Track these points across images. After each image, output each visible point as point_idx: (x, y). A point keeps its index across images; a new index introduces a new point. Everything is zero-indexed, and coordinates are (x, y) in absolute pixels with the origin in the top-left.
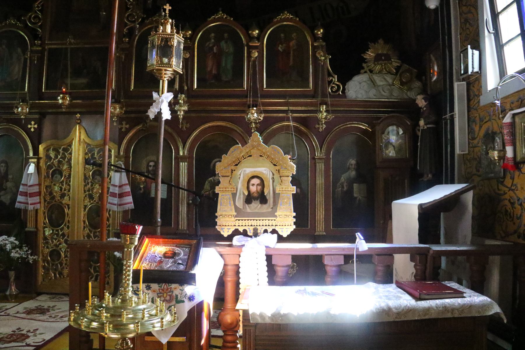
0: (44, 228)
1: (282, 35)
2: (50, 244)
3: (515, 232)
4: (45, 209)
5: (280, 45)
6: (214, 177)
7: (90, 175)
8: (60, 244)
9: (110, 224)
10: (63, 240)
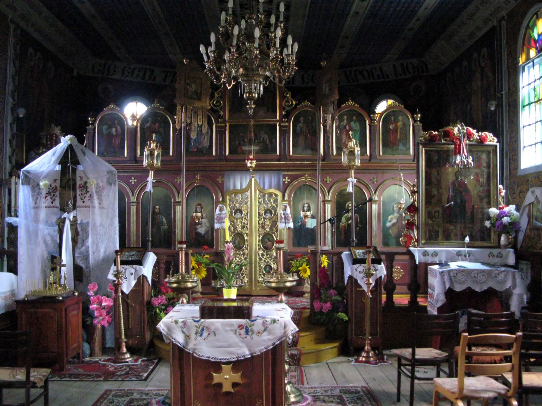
3: (532, 246)
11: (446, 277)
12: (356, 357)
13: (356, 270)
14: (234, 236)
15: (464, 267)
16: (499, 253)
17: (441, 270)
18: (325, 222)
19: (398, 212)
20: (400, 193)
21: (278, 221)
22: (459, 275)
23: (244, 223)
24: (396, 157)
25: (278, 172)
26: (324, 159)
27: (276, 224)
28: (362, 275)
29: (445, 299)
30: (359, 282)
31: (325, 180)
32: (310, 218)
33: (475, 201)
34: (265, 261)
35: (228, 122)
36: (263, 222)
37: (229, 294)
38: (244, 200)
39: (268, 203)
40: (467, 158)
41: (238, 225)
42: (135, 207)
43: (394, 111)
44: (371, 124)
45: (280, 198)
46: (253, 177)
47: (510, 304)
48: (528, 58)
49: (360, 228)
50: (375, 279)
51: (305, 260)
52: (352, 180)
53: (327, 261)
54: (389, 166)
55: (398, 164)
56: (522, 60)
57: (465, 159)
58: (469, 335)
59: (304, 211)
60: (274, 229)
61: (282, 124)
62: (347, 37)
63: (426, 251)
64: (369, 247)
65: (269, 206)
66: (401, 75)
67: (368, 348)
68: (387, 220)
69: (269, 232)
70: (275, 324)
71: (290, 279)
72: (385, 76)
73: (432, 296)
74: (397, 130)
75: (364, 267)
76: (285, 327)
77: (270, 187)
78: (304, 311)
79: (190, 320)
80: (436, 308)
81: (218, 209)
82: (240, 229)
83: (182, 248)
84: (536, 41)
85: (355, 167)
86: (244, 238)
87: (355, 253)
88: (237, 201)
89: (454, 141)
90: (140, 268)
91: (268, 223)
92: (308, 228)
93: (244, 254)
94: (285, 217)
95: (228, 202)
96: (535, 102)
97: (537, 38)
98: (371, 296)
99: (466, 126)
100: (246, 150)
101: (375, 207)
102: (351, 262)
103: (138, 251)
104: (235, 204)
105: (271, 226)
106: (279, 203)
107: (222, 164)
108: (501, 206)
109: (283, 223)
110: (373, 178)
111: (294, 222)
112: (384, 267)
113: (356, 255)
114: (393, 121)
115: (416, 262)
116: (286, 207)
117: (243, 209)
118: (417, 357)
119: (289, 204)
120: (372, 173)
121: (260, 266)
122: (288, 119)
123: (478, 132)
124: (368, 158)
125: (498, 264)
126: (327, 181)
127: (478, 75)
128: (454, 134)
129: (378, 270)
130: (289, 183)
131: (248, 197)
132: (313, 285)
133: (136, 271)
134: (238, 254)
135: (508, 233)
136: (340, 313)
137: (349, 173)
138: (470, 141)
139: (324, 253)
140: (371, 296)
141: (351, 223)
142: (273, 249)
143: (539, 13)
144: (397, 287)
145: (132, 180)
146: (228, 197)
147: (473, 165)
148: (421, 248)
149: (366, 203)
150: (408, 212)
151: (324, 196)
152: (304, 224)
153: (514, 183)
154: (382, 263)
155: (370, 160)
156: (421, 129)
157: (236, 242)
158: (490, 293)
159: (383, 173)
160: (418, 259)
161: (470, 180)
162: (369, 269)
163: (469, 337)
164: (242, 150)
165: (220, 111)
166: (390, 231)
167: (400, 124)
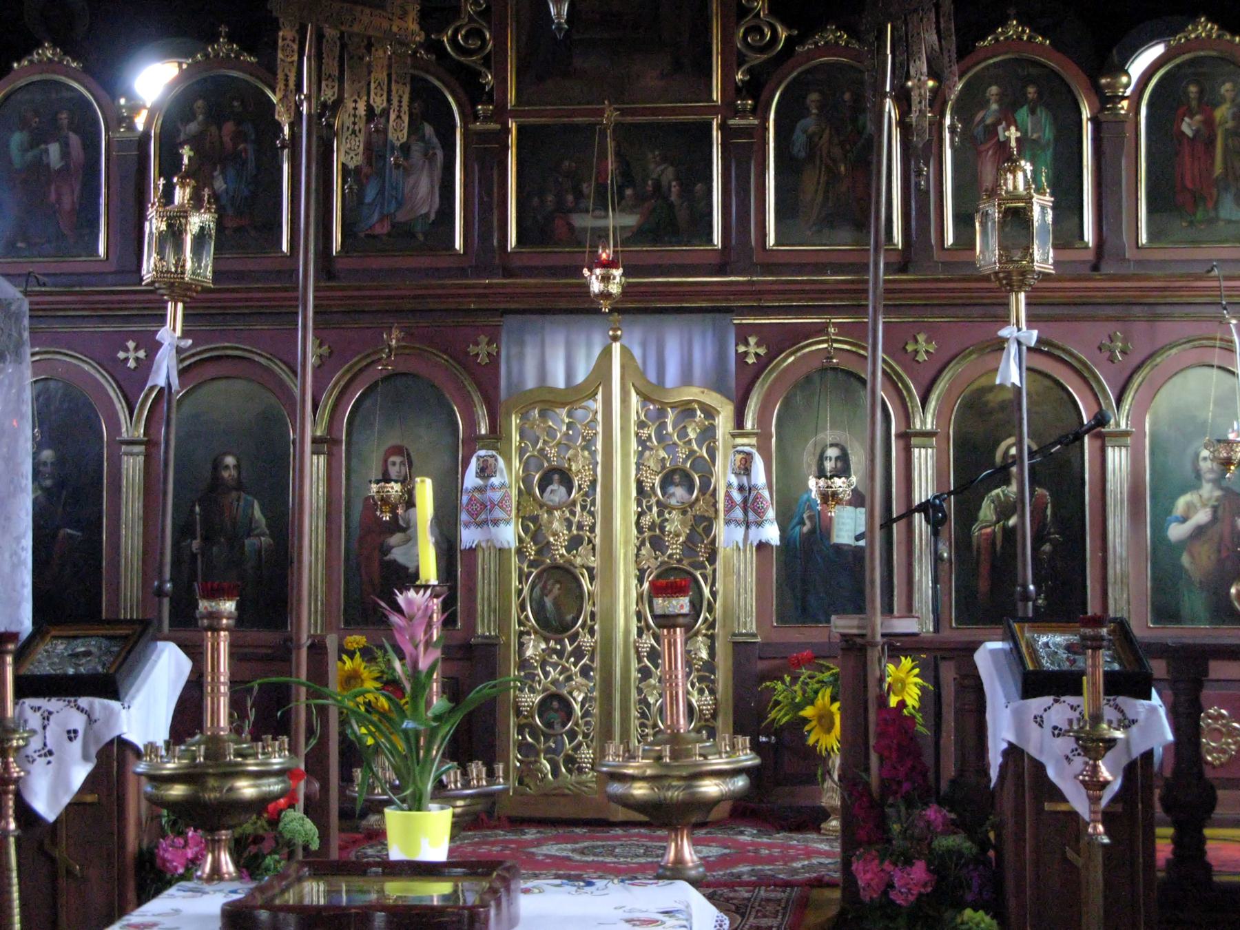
0: (521, 634)
1: (1193, 89)
2: (540, 682)
4: (520, 582)
5: (1187, 119)
6: (1005, 487)
7: (654, 484)
8: (569, 679)
9: (714, 620)
10: (575, 667)
13: (1039, 721)
14: (539, 576)
18: (908, 514)
19: (1218, 482)
23: (580, 527)
25: (717, 316)
26: (903, 262)
27: (708, 529)
28: (1065, 744)
30: (1051, 773)
31: (910, 348)
32: (850, 503)
35: (515, 114)
36: (658, 521)
37: (410, 835)
39: (675, 444)
42: (141, 458)
43: (1191, 63)
44: (1102, 117)
45: (724, 423)
46: (615, 338)
49: (1055, 544)
50: (1124, 762)
51: (826, 676)
53: (918, 680)
55: (1217, 279)
59: (821, 474)
60: (701, 549)
61: (731, 122)
64: (1097, 622)
65: (682, 454)
68: (1169, 511)
69: (679, 561)
74: (1210, 143)
77: (687, 379)
78: (815, 893)
82: (563, 551)
83: (215, 616)
86: (580, 586)
87: (1031, 647)
88: (551, 432)
90: (106, 708)
91: (675, 523)
93: (578, 654)
94: (745, 501)
95: (515, 437)
98: (1106, 840)
100: (584, 230)
101: (1117, 459)
102: (1014, 688)
103: (109, 638)
104: (542, 450)
106: (720, 444)
109: (738, 523)
112: (1162, 712)
114: (1194, 103)
116: (748, 458)
119: (764, 450)
120: (1108, 319)
121: (644, 702)
122: (756, 98)
124: (1090, 256)
126: (916, 352)
129: (1134, 722)
130: (763, 364)
131: (594, 420)
132: (851, 782)
133: (91, 721)
134: (555, 651)
136: (968, 912)
139: (898, 647)
140: (1106, 840)
141: (1014, 528)
144: (1221, 794)
145: (126, 350)
146: (515, 421)
149: (1079, 438)
151: (907, 417)
152: (822, 529)
155: (1096, 267)
157: (548, 601)
159: (1154, 319)
162: (1096, 718)
164: (571, 228)
166: (1185, 560)
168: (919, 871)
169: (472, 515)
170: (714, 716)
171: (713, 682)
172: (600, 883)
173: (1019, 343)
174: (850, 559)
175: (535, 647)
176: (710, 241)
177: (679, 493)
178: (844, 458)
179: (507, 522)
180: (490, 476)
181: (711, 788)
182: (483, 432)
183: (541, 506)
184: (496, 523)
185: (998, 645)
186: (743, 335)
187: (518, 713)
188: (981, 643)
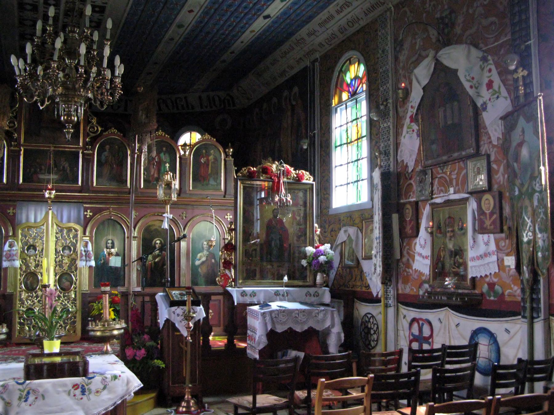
8: (34, 304)
11: (268, 318)
12: (175, 408)
13: (174, 313)
14: (26, 275)
15: (285, 308)
16: (316, 292)
17: (263, 311)
19: (208, 250)
20: (211, 229)
21: (77, 259)
22: (281, 316)
24: (206, 192)
25: (78, 204)
27: (75, 262)
29: (267, 341)
30: (177, 325)
33: (292, 239)
34: (61, 303)
35: (23, 146)
37: (51, 347)
38: (38, 235)
39: (66, 239)
40: (286, 196)
41: (31, 263)
43: (204, 144)
45: (80, 233)
46: (50, 209)
47: (328, 343)
48: (340, 101)
52: (168, 215)
54: (200, 201)
56: (335, 101)
57: (284, 197)
58: (326, 380)
59: (107, 248)
60: (73, 267)
62: (156, 63)
63: (244, 291)
66: (206, 107)
67: (188, 397)
69: (67, 271)
70: (117, 380)
71: (118, 326)
72: (190, 107)
73: (252, 339)
75: (182, 309)
76: (128, 382)
77: (69, 221)
79: (12, 383)
80: (258, 351)
81: (7, 244)
82: (33, 268)
84: (348, 86)
85: (171, 202)
89: (273, 178)
91: (66, 261)
92: (111, 267)
93: (37, 297)
94: (86, 255)
95: (20, 236)
96: (347, 143)
97: (349, 82)
98: (191, 341)
99: (285, 164)
104: (27, 240)
105: (70, 264)
106: (79, 239)
107: (13, 193)
108: (316, 245)
109: (84, 261)
110: (183, 213)
111: (96, 260)
112: (203, 309)
113: (173, 297)
115: (234, 303)
117: (37, 245)
118: (258, 405)
119: (91, 240)
120: (181, 208)
123: (295, 170)
124: (223, 193)
125: (315, 303)
127: (289, 113)
128: (272, 172)
130: (91, 217)
131: (43, 232)
135: (323, 272)
137: (164, 208)
138: (287, 179)
140: (191, 341)
142: (71, 291)
143: (352, 59)
146: (20, 231)
147: (291, 203)
148: (239, 288)
150: (225, 250)
152: (106, 262)
153: (325, 222)
154: (201, 305)
156: (233, 164)
157: (29, 282)
158: (311, 332)
160: (236, 299)
161: (287, 219)
162: (189, 312)
163: (326, 382)
164: (39, 179)
165: (14, 132)
166: (200, 270)
167: (211, 158)
168: (143, 351)
169: (7, 258)
170: (76, 313)
171: (75, 304)
172: (94, 356)
173: (168, 218)
174: (114, 270)
175: (24, 295)
176: (78, 184)
177: (67, 252)
178: (113, 243)
179: (17, 260)
180: (13, 247)
181: (116, 332)
182: (11, 234)
183: (27, 255)
184: (14, 260)
185: (162, 294)
186: (86, 209)
187: (19, 313)
188: (157, 293)
